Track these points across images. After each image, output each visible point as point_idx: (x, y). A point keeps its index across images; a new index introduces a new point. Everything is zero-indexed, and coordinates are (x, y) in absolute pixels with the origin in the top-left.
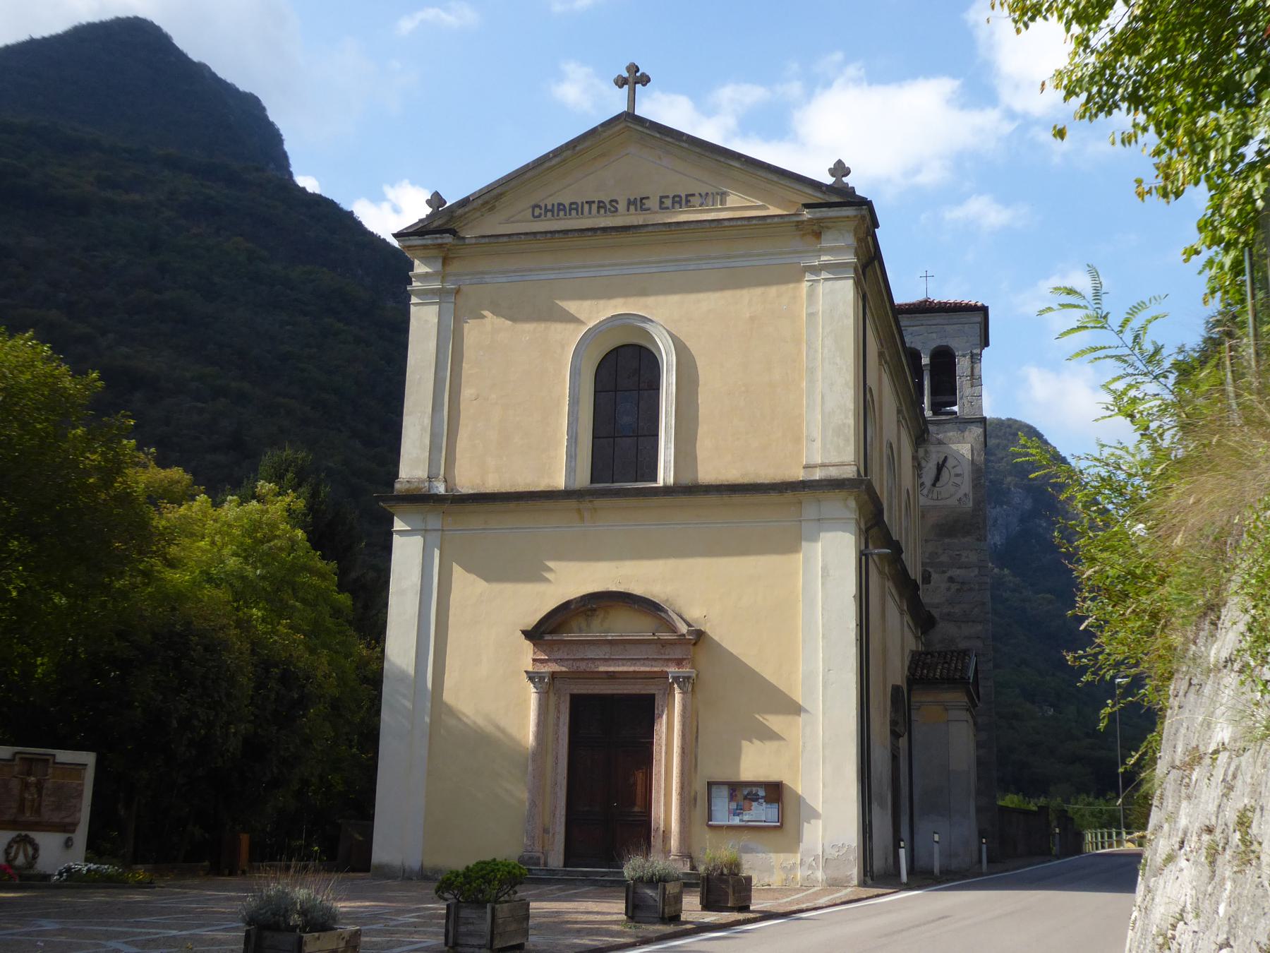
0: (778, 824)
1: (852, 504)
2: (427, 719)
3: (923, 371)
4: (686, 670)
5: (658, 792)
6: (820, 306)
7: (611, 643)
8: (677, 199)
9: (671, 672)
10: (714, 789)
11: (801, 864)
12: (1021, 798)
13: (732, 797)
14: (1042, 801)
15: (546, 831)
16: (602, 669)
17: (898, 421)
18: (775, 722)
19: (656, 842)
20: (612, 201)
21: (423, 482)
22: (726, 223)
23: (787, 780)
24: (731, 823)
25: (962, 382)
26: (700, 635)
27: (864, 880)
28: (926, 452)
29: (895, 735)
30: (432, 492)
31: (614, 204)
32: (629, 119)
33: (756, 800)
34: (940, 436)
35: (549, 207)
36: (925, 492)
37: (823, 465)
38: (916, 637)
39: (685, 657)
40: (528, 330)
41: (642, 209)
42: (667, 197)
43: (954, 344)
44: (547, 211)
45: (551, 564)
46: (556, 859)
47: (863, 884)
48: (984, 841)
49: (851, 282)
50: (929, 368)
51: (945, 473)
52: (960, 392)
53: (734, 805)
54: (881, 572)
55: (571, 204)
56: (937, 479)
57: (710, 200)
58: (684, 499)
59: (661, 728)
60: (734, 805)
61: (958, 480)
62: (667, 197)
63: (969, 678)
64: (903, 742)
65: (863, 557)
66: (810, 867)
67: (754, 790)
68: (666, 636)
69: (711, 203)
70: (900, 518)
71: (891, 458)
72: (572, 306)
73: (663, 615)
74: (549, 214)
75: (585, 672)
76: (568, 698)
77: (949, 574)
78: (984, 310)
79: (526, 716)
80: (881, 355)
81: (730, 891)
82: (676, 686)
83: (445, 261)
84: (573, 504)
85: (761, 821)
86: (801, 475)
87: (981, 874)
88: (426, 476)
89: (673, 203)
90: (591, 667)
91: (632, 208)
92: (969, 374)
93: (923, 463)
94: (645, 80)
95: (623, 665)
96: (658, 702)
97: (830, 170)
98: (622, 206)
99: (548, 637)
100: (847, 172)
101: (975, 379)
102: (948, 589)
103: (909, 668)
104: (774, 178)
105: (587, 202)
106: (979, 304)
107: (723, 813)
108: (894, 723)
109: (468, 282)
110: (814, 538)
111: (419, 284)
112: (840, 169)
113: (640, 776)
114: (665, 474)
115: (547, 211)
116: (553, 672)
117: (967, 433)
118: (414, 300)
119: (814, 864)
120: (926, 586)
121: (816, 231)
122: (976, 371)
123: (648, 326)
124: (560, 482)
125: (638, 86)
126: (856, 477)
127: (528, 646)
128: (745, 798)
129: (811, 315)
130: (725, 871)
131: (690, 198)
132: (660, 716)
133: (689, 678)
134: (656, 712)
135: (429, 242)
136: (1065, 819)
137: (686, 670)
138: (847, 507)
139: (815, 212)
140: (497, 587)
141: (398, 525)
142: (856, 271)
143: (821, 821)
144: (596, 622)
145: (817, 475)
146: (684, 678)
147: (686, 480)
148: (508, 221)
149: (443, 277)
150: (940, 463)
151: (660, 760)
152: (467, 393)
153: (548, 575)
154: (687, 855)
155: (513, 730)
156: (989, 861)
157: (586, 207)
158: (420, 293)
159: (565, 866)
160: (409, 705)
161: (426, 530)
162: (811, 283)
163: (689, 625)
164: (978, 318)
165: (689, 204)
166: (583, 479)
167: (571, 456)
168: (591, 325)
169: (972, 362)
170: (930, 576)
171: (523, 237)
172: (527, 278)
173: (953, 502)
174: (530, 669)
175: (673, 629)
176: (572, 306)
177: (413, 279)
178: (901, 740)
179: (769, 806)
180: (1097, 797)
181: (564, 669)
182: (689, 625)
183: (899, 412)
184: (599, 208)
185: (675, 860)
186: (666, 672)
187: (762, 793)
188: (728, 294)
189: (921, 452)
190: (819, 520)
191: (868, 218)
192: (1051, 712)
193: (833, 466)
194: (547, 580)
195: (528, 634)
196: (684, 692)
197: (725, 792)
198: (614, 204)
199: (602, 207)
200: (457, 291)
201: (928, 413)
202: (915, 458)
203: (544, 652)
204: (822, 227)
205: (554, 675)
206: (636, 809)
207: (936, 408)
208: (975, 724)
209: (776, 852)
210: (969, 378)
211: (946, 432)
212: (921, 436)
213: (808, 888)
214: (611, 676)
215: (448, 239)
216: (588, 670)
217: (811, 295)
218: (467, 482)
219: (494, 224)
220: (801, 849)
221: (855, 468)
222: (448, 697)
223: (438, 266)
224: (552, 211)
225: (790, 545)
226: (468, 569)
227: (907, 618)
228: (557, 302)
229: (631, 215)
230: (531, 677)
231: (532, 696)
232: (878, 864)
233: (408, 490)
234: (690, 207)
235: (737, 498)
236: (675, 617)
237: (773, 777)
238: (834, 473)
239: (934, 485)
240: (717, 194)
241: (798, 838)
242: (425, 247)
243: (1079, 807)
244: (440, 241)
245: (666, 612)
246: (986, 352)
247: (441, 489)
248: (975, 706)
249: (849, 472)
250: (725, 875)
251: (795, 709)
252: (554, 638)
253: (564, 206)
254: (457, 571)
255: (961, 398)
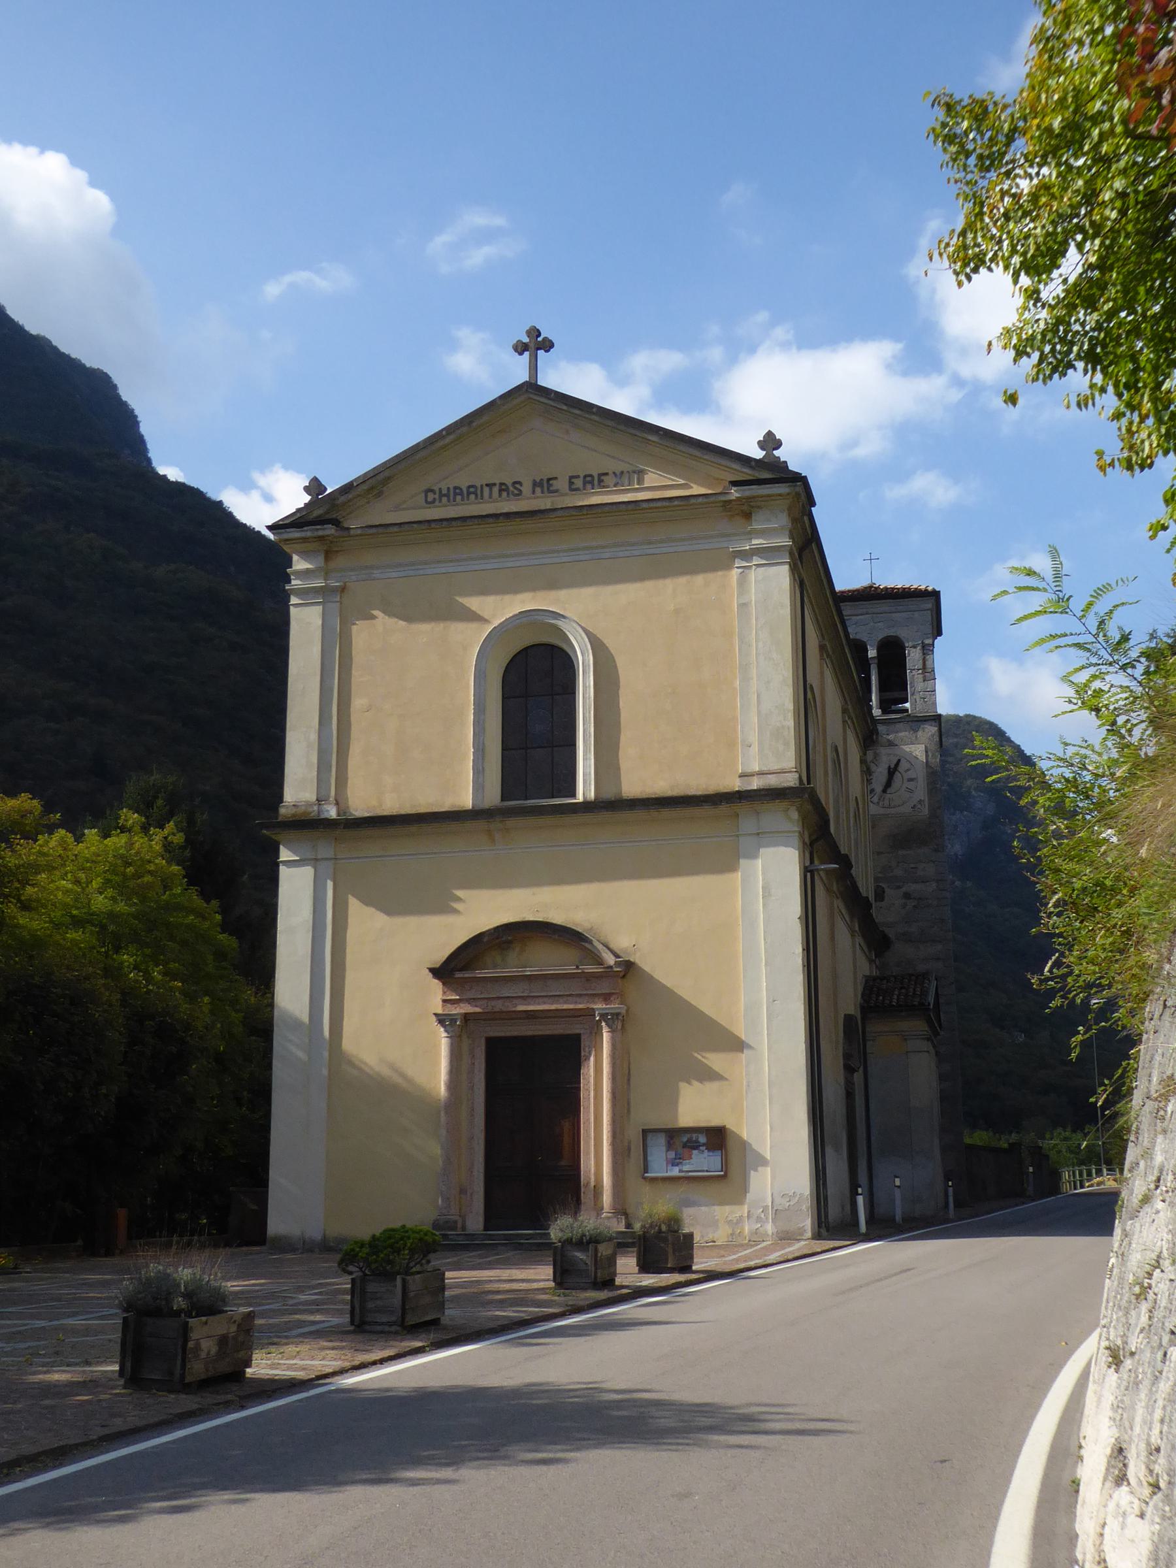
0: (722, 1173)
1: (795, 815)
2: (325, 1072)
3: (870, 665)
4: (614, 1006)
5: (588, 1143)
6: (753, 595)
7: (530, 978)
8: (588, 479)
9: (597, 1009)
10: (650, 1136)
11: (749, 1217)
12: (991, 1134)
13: (670, 1146)
14: (1014, 1137)
15: (463, 1191)
16: (521, 1008)
17: (844, 722)
18: (715, 1060)
19: (586, 1197)
20: (515, 483)
21: (310, 805)
22: (645, 505)
23: (731, 1125)
24: (669, 1174)
25: (913, 676)
26: (629, 967)
27: (819, 1232)
28: (876, 755)
29: (849, 1069)
30: (322, 817)
31: (518, 486)
32: (531, 390)
33: (696, 1148)
34: (891, 737)
35: (444, 491)
36: (875, 799)
37: (761, 773)
38: (871, 961)
39: (613, 991)
40: (425, 630)
41: (550, 491)
42: (578, 477)
43: (903, 633)
44: (441, 495)
45: (459, 893)
46: (475, 1222)
47: (817, 1236)
48: (950, 1183)
49: (786, 568)
50: (876, 661)
51: (897, 776)
52: (911, 688)
53: (672, 1155)
54: (828, 890)
55: (469, 487)
56: (888, 784)
57: (626, 476)
58: (606, 815)
59: (588, 1071)
60: (672, 1155)
61: (911, 785)
62: (578, 477)
63: (929, 1004)
64: (858, 1077)
65: (809, 874)
66: (759, 1219)
67: (694, 1136)
68: (591, 969)
69: (626, 482)
70: (849, 828)
71: (837, 762)
72: (474, 603)
73: (587, 945)
74: (444, 499)
75: (502, 1012)
76: (483, 1041)
77: (904, 889)
78: (935, 595)
79: (438, 1063)
80: (822, 648)
81: (670, 1250)
82: (603, 1024)
83: (327, 558)
84: (481, 824)
85: (703, 1171)
86: (736, 785)
87: (947, 1221)
88: (314, 798)
89: (584, 484)
90: (509, 1007)
91: (538, 490)
92: (921, 667)
93: (873, 768)
94: (548, 345)
95: (545, 1003)
96: (585, 1042)
97: (759, 442)
98: (526, 488)
99: (458, 975)
100: (778, 444)
101: (928, 673)
102: (904, 906)
103: (863, 995)
104: (697, 453)
105: (487, 485)
106: (930, 589)
107: (660, 1165)
108: (847, 1056)
109: (354, 578)
110: (754, 856)
111: (300, 582)
112: (770, 442)
113: (566, 1125)
114: (585, 788)
115: (441, 495)
116: (466, 1014)
117: (920, 733)
118: (294, 600)
119: (763, 1216)
120: (878, 904)
121: (745, 511)
122: (928, 664)
123: (560, 623)
124: (466, 800)
125: (541, 353)
126: (798, 785)
127: (437, 985)
128: (685, 1146)
129: (743, 606)
130: (664, 1228)
131: (602, 478)
132: (588, 1058)
133: (618, 1014)
134: (583, 1054)
135: (309, 534)
136: (1039, 1156)
137: (614, 1006)
138: (788, 820)
139: (744, 490)
140: (399, 921)
141: (285, 854)
142: (791, 554)
143: (769, 1169)
144: (513, 956)
145: (755, 784)
146: (612, 1014)
147: (609, 794)
148: (397, 508)
149: (327, 574)
150: (892, 766)
151: (588, 1107)
152: (358, 703)
153: (456, 906)
154: (621, 1210)
155: (421, 1079)
156: (955, 1206)
157: (486, 490)
158: (300, 593)
159: (486, 1229)
160: (301, 1054)
161: (316, 860)
162: (740, 570)
163: (617, 956)
164: (929, 604)
165: (602, 484)
166: (493, 796)
167: (479, 771)
168: (496, 623)
169: (924, 654)
170: (884, 892)
171: (415, 525)
172: (421, 572)
173: (906, 809)
174: (440, 1011)
175: (599, 961)
176: (474, 603)
177: (292, 577)
178: (855, 1074)
179: (711, 1154)
180: (1074, 1131)
181: (478, 1010)
182: (617, 956)
183: (845, 711)
184: (501, 491)
185: (609, 1218)
186: (593, 1009)
187: (702, 1139)
188: (649, 584)
189: (870, 755)
190: (758, 834)
191: (803, 495)
192: (1022, 1038)
193: (773, 773)
194: (455, 911)
195: (436, 972)
196: (612, 1031)
197: (662, 1140)
198: (518, 486)
199: (504, 490)
200: (343, 589)
201: (876, 712)
202: (863, 761)
203: (455, 991)
204: (753, 507)
205: (466, 1017)
206: (563, 1163)
207: (885, 706)
208: (937, 1053)
209: (721, 1204)
210: (920, 671)
211: (897, 732)
212: (869, 737)
213: (757, 1243)
214: (531, 1016)
215: (330, 530)
216: (505, 1010)
217: (742, 582)
218: (362, 802)
219: (380, 513)
220: (747, 1201)
221: (796, 775)
222: (348, 1044)
223: (320, 561)
224: (447, 495)
225: (728, 865)
226: (367, 901)
227: (859, 940)
228: (460, 600)
229: (538, 497)
230: (441, 1019)
231: (443, 1041)
232: (834, 1212)
233: (294, 815)
234: (604, 487)
235: (666, 813)
236: (600, 947)
237: (715, 1122)
238: (773, 781)
239: (884, 791)
240: (634, 472)
241: (745, 1189)
242: (304, 540)
243: (1054, 1142)
244: (320, 533)
245: (590, 942)
246: (939, 641)
247: (332, 812)
248: (936, 1034)
249: (791, 780)
250: (664, 1232)
251: (737, 1045)
252: (466, 975)
253: (461, 489)
254: (354, 904)
255: (913, 694)
